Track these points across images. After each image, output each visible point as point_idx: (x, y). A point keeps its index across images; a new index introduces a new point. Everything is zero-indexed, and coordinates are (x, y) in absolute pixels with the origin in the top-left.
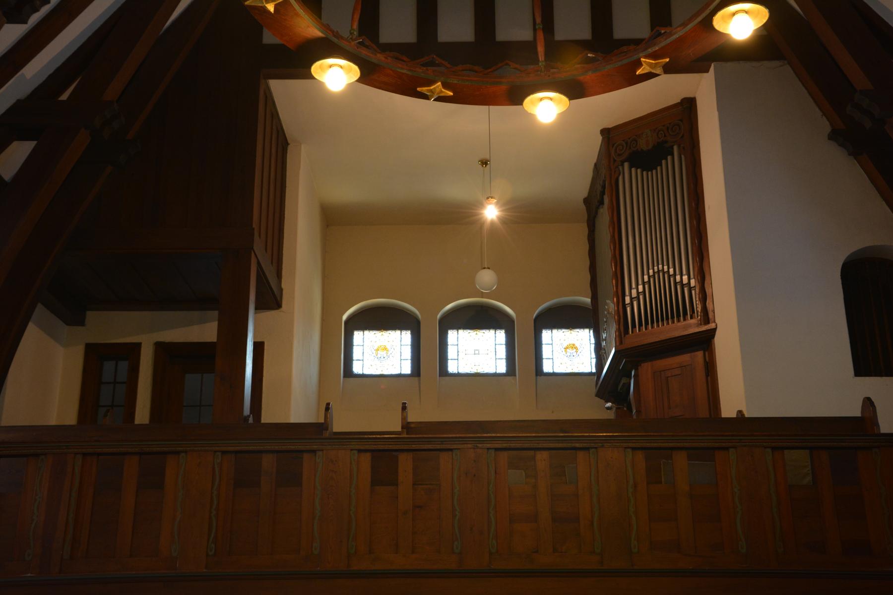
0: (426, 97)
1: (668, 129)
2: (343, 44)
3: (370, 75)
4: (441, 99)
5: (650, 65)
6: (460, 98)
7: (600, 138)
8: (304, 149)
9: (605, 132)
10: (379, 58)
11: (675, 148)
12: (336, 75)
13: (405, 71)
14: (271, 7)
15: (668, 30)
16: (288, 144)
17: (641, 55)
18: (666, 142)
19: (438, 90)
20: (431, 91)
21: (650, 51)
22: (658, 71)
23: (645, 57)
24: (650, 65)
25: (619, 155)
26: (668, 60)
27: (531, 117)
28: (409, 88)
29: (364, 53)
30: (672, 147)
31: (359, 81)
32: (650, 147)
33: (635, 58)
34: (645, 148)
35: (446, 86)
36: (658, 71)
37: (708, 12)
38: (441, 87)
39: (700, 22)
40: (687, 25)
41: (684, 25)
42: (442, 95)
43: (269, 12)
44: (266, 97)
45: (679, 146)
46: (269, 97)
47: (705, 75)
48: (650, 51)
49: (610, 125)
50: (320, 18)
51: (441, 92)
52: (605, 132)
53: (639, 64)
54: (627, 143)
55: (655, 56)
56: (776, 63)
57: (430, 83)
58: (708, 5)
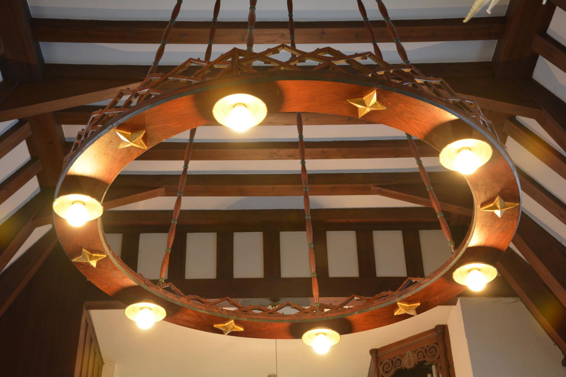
0: (220, 332)
1: (426, 350)
2: (153, 290)
3: (174, 314)
4: (233, 334)
5: (405, 308)
6: (250, 332)
7: (370, 357)
8: (117, 366)
9: (374, 352)
10: (182, 301)
11: (434, 367)
12: (145, 316)
13: (203, 312)
14: (94, 263)
15: (418, 280)
16: (103, 364)
17: (397, 300)
18: (425, 362)
19: (231, 327)
20: (225, 327)
21: (404, 297)
22: (412, 312)
23: (401, 302)
24: (405, 308)
25: (387, 372)
26: (419, 304)
27: (308, 349)
28: (208, 325)
29: (170, 297)
30: (431, 366)
31: (165, 319)
32: (412, 366)
33: (392, 302)
34: (408, 367)
35: (237, 322)
36: (412, 312)
37: (448, 268)
38: (234, 324)
39: (443, 276)
40: (432, 277)
41: (431, 277)
42: (235, 330)
43: (92, 267)
44: (87, 324)
45: (437, 366)
46: (89, 325)
47: (453, 307)
48: (404, 297)
49: (378, 347)
50: (136, 271)
51: (234, 328)
52: (374, 352)
53: (395, 307)
54: (392, 362)
55: (409, 301)
56: (511, 299)
57: (225, 320)
58: (447, 263)
